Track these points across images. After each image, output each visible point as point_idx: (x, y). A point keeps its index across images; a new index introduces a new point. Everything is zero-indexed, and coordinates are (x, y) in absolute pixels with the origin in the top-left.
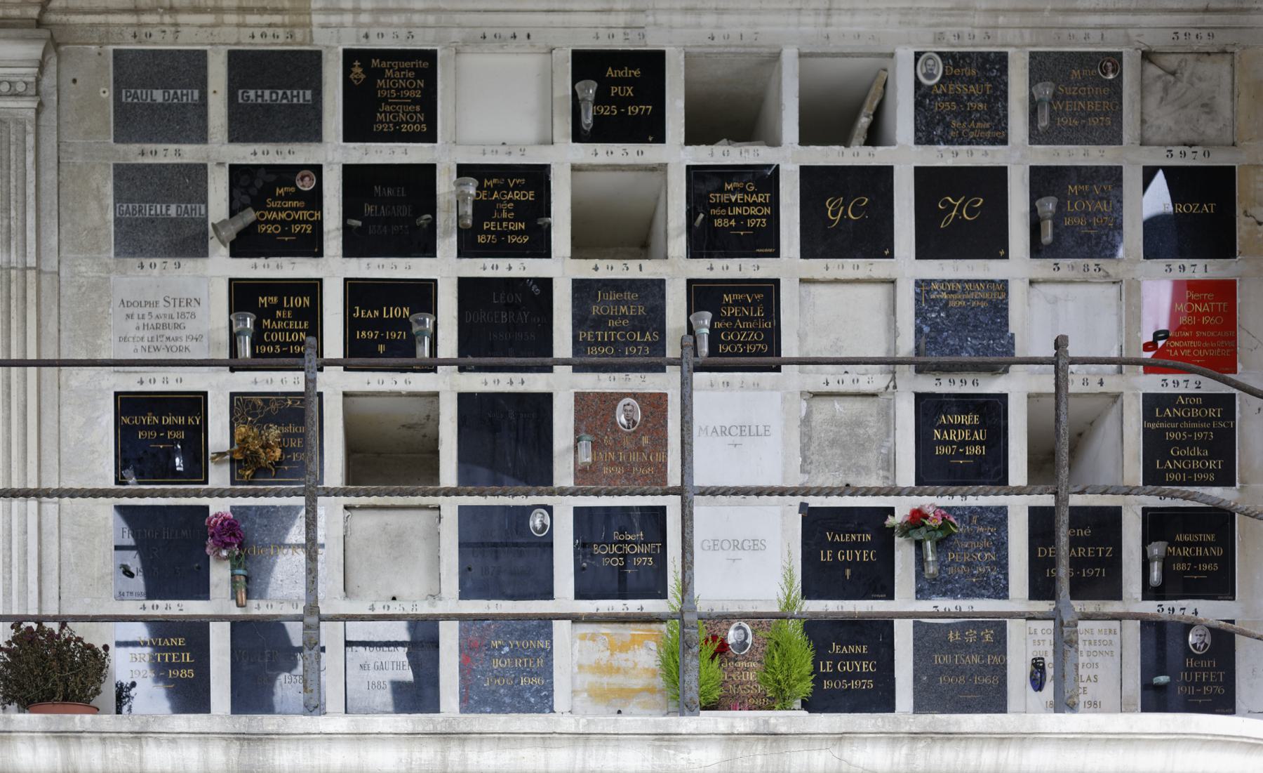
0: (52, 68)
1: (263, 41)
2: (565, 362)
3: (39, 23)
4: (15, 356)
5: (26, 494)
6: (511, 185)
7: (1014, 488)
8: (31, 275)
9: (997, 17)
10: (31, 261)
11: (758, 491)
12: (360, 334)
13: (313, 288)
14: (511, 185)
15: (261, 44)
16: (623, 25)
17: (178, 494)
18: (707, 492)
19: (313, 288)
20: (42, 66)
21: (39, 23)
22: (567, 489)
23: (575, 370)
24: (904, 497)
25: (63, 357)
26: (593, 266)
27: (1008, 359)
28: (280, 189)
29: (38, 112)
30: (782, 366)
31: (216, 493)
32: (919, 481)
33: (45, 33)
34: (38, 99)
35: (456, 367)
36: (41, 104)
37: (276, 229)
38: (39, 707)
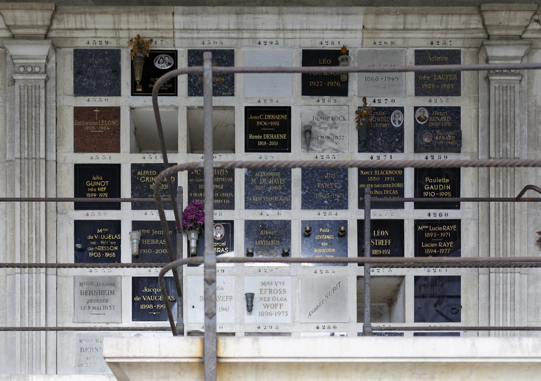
0: (53, 59)
2: (409, 200)
8: (43, 162)
15: (437, 47)
20: (48, 59)
21: (46, 37)
26: (370, 157)
27: (398, 199)
28: (100, 230)
29: (46, 82)
34: (46, 75)
36: (48, 78)
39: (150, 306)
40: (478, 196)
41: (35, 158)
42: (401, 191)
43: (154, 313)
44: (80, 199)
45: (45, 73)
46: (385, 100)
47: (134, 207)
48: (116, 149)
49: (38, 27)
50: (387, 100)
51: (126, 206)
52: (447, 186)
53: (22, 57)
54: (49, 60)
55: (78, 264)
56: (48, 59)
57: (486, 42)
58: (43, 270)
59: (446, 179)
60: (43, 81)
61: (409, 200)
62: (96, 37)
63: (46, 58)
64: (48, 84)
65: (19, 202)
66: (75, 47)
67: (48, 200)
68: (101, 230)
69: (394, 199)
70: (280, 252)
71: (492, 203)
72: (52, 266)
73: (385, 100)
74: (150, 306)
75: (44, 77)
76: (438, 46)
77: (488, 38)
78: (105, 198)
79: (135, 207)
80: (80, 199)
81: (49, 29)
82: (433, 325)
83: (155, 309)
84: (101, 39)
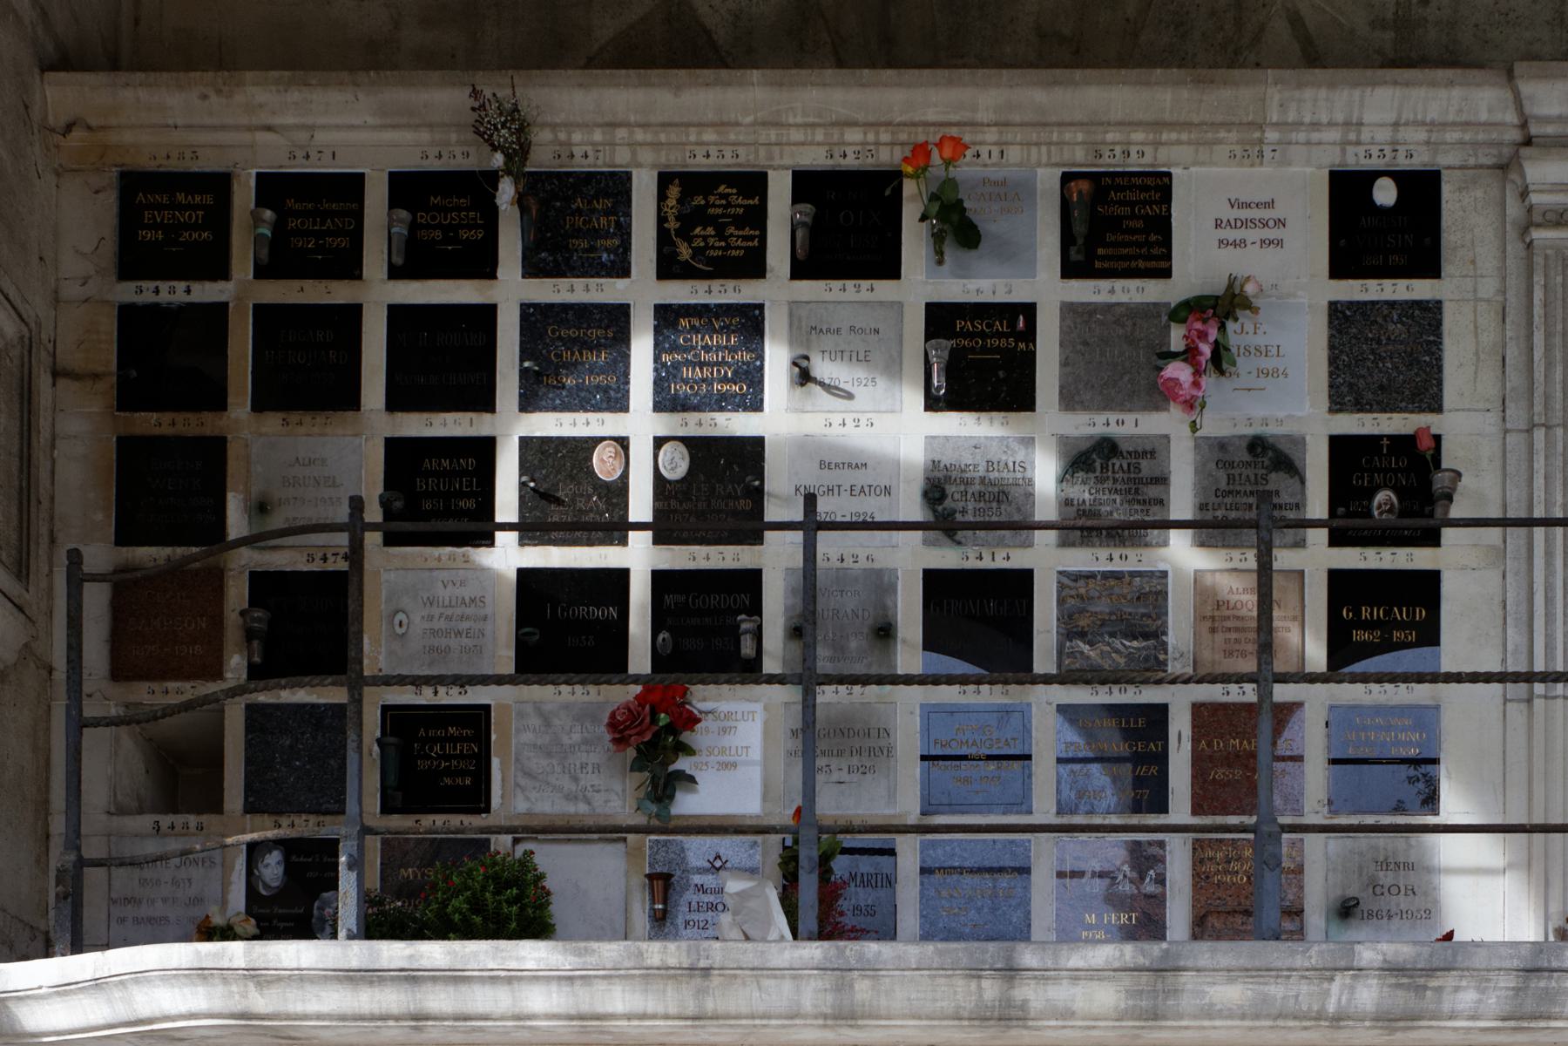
1: (306, 163)
2: (374, 527)
18: (1441, 678)
23: (522, 543)
31: (1234, 679)
35: (648, 535)
40: (1505, 511)
47: (657, 541)
55: (524, 677)
57: (1525, 151)
61: (374, 527)
62: (722, 144)
65: (1543, 528)
67: (1509, 522)
71: (1539, 532)
72: (1516, 678)
76: (293, 162)
79: (1337, 540)
80: (397, 526)
82: (1220, 820)
84: (1383, 147)
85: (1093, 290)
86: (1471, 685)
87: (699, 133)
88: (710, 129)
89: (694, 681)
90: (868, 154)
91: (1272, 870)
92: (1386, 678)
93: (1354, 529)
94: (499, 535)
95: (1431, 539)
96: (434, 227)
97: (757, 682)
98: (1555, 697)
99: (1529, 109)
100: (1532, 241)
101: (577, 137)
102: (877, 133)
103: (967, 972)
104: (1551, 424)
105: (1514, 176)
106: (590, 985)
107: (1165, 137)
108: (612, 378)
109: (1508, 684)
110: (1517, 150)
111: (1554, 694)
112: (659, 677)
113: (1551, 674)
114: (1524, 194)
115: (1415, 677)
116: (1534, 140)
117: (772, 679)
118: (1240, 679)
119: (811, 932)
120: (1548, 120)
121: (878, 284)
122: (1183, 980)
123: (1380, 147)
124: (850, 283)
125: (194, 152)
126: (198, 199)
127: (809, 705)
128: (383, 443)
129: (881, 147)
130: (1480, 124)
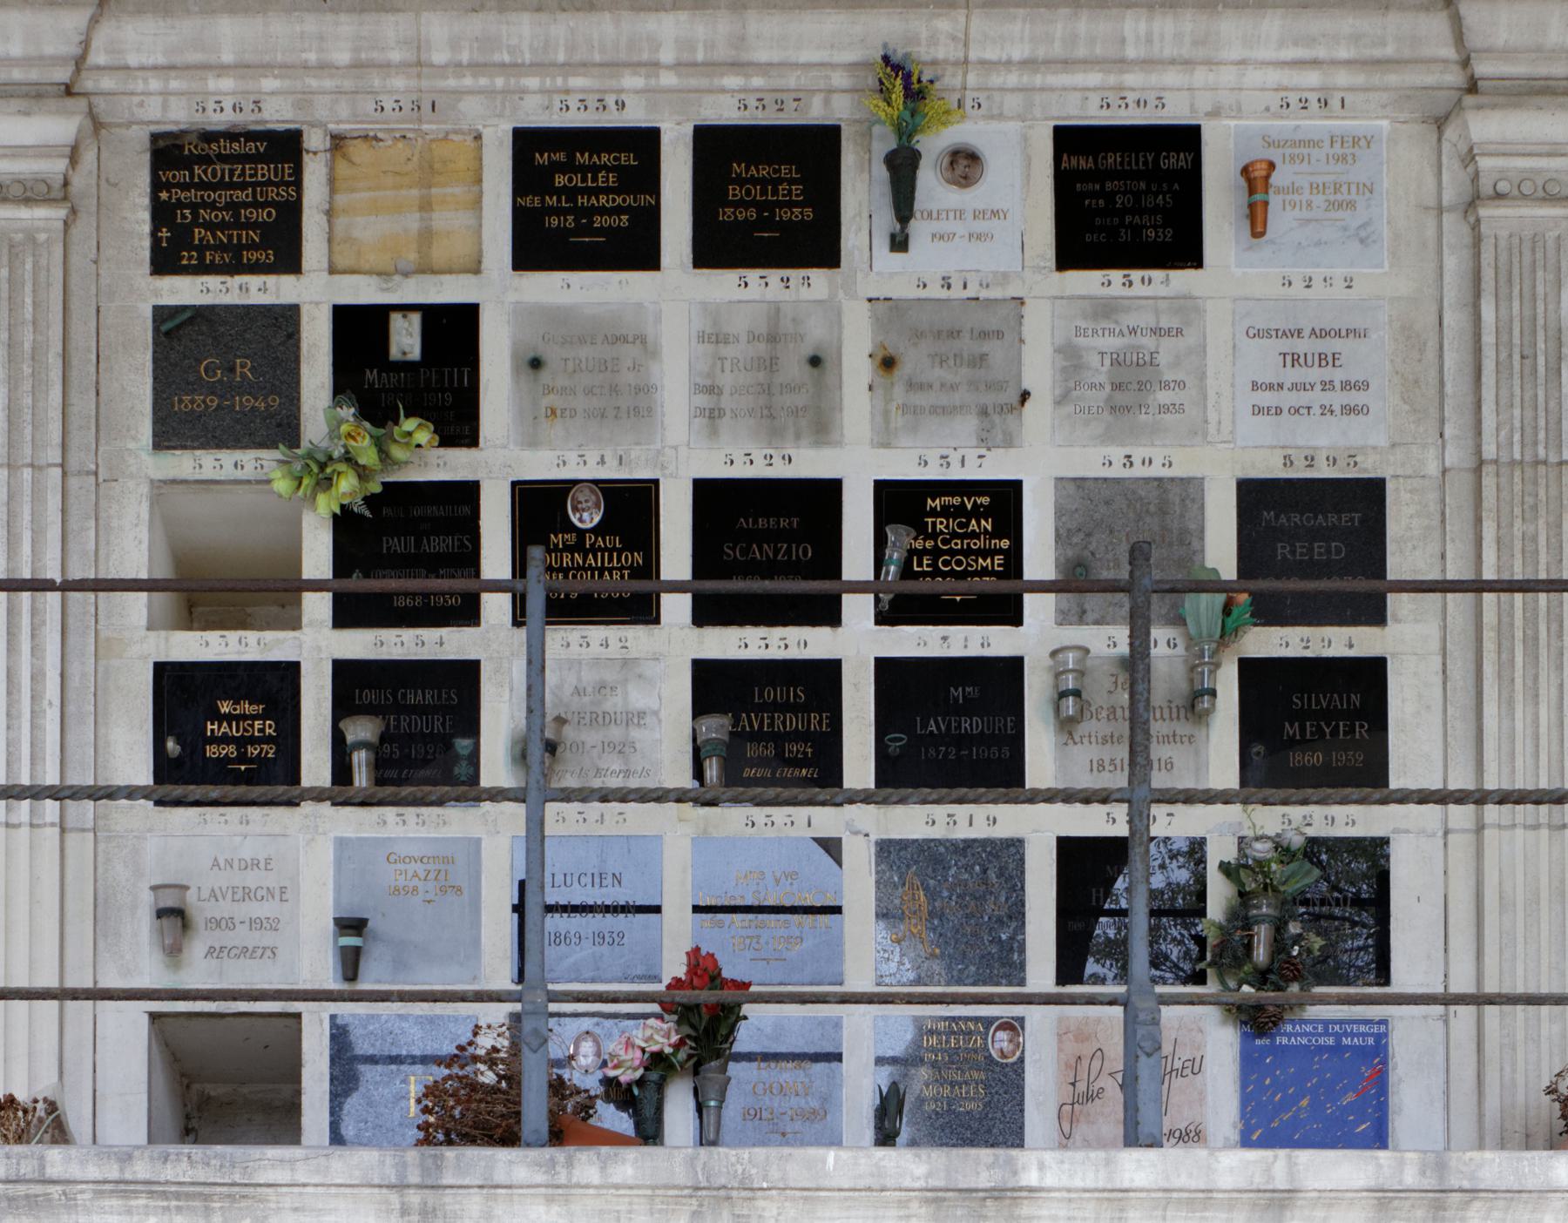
0: (88, 157)
3: (69, 91)
4: (26, 596)
5: (36, 793)
6: (969, 507)
7: (312, 789)
9: (167, 80)
10: (54, 455)
11: (1049, 795)
12: (927, 752)
13: (826, 675)
14: (969, 507)
16: (1222, 67)
17: (610, 798)
19: (826, 675)
21: (69, 91)
22: (138, 788)
24: (1412, 807)
25: (91, 596)
27: (1361, 585)
30: (845, 596)
31: (673, 796)
32: (881, 781)
33: (82, 103)
36: (74, 211)
37: (269, 214)
38: (157, 1058)
39: (230, 750)
41: (1521, 462)
42: (649, 567)
43: (243, 768)
44: (710, 586)
45: (65, 198)
46: (795, 100)
48: (887, 670)
49: (40, 60)
50: (799, 100)
51: (858, 609)
52: (983, 522)
53: (229, 586)
54: (76, 162)
56: (74, 155)
57: (1469, 100)
58: (50, 807)
59: (250, 704)
60: (60, 225)
63: (68, 151)
64: (74, 231)
66: (1058, 118)
68: (989, 561)
69: (988, 584)
70: (915, 454)
73: (795, 100)
74: (230, 750)
75: (61, 212)
77: (1472, 87)
78: (617, 584)
79: (348, 614)
80: (710, 586)
81: (80, 62)
83: (242, 758)
84: (1305, 95)
85: (1281, 282)
86: (1048, 805)
87: (565, 79)
88: (1202, 67)
89: (1253, 799)
90: (1120, 102)
91: (1149, 1055)
92: (632, 797)
93: (406, 594)
94: (848, 600)
95: (1373, 612)
96: (263, 205)
97: (1384, 802)
98: (19, 825)
99: (1474, 40)
100: (1478, 220)
101: (972, 79)
102: (145, 80)
103: (929, 1194)
104: (43, 462)
105: (1450, 133)
106: (567, 1200)
107: (717, 82)
108: (274, 400)
109: (1451, 806)
110: (1460, 100)
111: (40, 822)
112: (336, 788)
113: (102, 788)
114: (1469, 157)
115: (1415, 795)
116: (1480, 83)
117: (497, 795)
118: (1104, 797)
119: (1226, 1139)
120: (1507, 53)
121: (1176, 275)
122: (447, 1200)
123: (759, 95)
124: (753, 275)
125: (1160, 98)
126: (605, 158)
127: (536, 827)
128: (470, 478)
129: (172, 98)
130: (595, 65)
